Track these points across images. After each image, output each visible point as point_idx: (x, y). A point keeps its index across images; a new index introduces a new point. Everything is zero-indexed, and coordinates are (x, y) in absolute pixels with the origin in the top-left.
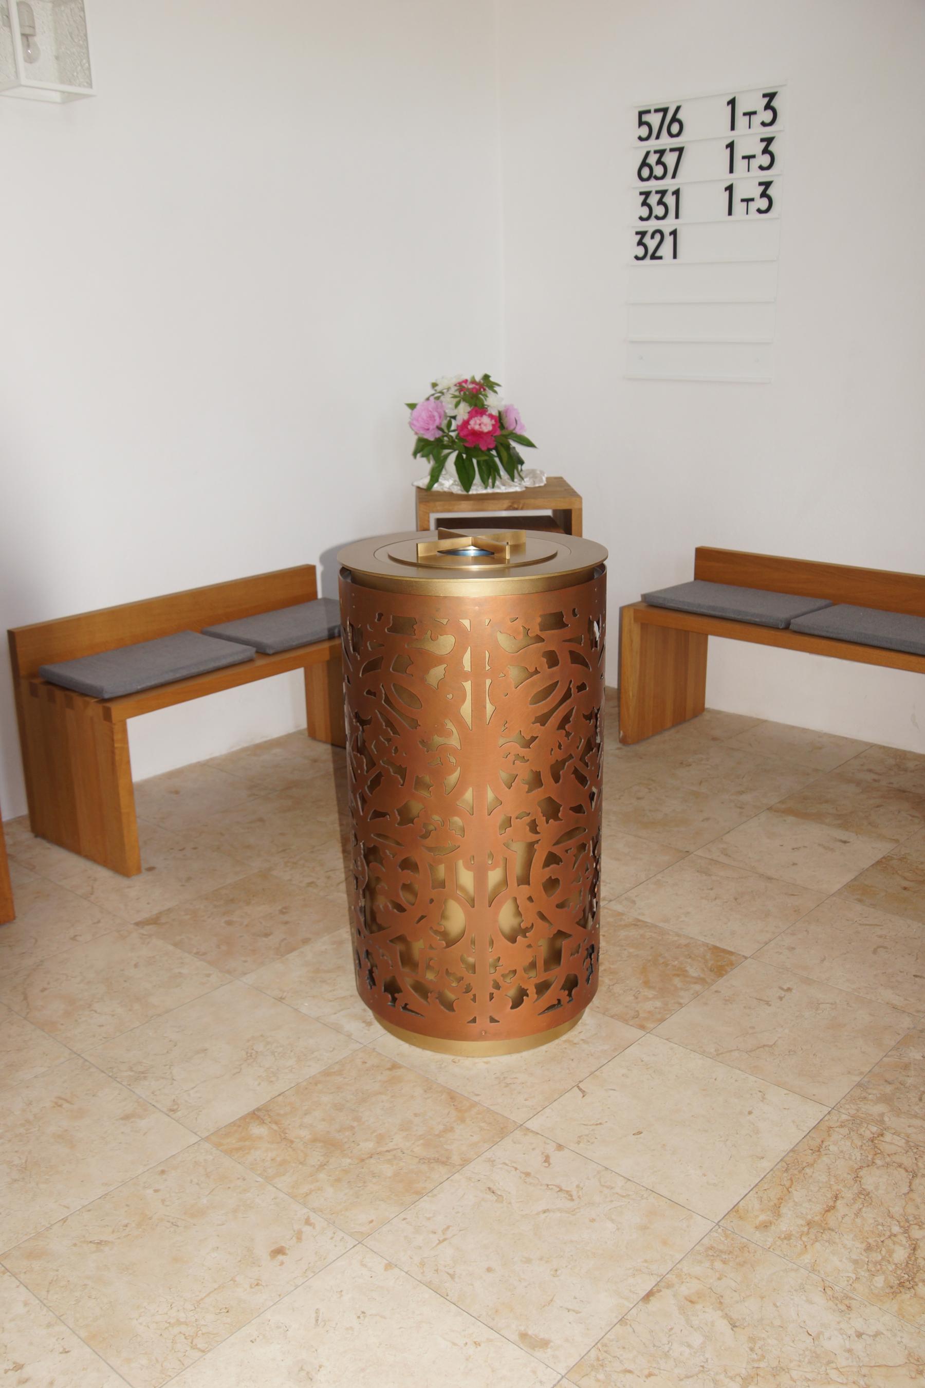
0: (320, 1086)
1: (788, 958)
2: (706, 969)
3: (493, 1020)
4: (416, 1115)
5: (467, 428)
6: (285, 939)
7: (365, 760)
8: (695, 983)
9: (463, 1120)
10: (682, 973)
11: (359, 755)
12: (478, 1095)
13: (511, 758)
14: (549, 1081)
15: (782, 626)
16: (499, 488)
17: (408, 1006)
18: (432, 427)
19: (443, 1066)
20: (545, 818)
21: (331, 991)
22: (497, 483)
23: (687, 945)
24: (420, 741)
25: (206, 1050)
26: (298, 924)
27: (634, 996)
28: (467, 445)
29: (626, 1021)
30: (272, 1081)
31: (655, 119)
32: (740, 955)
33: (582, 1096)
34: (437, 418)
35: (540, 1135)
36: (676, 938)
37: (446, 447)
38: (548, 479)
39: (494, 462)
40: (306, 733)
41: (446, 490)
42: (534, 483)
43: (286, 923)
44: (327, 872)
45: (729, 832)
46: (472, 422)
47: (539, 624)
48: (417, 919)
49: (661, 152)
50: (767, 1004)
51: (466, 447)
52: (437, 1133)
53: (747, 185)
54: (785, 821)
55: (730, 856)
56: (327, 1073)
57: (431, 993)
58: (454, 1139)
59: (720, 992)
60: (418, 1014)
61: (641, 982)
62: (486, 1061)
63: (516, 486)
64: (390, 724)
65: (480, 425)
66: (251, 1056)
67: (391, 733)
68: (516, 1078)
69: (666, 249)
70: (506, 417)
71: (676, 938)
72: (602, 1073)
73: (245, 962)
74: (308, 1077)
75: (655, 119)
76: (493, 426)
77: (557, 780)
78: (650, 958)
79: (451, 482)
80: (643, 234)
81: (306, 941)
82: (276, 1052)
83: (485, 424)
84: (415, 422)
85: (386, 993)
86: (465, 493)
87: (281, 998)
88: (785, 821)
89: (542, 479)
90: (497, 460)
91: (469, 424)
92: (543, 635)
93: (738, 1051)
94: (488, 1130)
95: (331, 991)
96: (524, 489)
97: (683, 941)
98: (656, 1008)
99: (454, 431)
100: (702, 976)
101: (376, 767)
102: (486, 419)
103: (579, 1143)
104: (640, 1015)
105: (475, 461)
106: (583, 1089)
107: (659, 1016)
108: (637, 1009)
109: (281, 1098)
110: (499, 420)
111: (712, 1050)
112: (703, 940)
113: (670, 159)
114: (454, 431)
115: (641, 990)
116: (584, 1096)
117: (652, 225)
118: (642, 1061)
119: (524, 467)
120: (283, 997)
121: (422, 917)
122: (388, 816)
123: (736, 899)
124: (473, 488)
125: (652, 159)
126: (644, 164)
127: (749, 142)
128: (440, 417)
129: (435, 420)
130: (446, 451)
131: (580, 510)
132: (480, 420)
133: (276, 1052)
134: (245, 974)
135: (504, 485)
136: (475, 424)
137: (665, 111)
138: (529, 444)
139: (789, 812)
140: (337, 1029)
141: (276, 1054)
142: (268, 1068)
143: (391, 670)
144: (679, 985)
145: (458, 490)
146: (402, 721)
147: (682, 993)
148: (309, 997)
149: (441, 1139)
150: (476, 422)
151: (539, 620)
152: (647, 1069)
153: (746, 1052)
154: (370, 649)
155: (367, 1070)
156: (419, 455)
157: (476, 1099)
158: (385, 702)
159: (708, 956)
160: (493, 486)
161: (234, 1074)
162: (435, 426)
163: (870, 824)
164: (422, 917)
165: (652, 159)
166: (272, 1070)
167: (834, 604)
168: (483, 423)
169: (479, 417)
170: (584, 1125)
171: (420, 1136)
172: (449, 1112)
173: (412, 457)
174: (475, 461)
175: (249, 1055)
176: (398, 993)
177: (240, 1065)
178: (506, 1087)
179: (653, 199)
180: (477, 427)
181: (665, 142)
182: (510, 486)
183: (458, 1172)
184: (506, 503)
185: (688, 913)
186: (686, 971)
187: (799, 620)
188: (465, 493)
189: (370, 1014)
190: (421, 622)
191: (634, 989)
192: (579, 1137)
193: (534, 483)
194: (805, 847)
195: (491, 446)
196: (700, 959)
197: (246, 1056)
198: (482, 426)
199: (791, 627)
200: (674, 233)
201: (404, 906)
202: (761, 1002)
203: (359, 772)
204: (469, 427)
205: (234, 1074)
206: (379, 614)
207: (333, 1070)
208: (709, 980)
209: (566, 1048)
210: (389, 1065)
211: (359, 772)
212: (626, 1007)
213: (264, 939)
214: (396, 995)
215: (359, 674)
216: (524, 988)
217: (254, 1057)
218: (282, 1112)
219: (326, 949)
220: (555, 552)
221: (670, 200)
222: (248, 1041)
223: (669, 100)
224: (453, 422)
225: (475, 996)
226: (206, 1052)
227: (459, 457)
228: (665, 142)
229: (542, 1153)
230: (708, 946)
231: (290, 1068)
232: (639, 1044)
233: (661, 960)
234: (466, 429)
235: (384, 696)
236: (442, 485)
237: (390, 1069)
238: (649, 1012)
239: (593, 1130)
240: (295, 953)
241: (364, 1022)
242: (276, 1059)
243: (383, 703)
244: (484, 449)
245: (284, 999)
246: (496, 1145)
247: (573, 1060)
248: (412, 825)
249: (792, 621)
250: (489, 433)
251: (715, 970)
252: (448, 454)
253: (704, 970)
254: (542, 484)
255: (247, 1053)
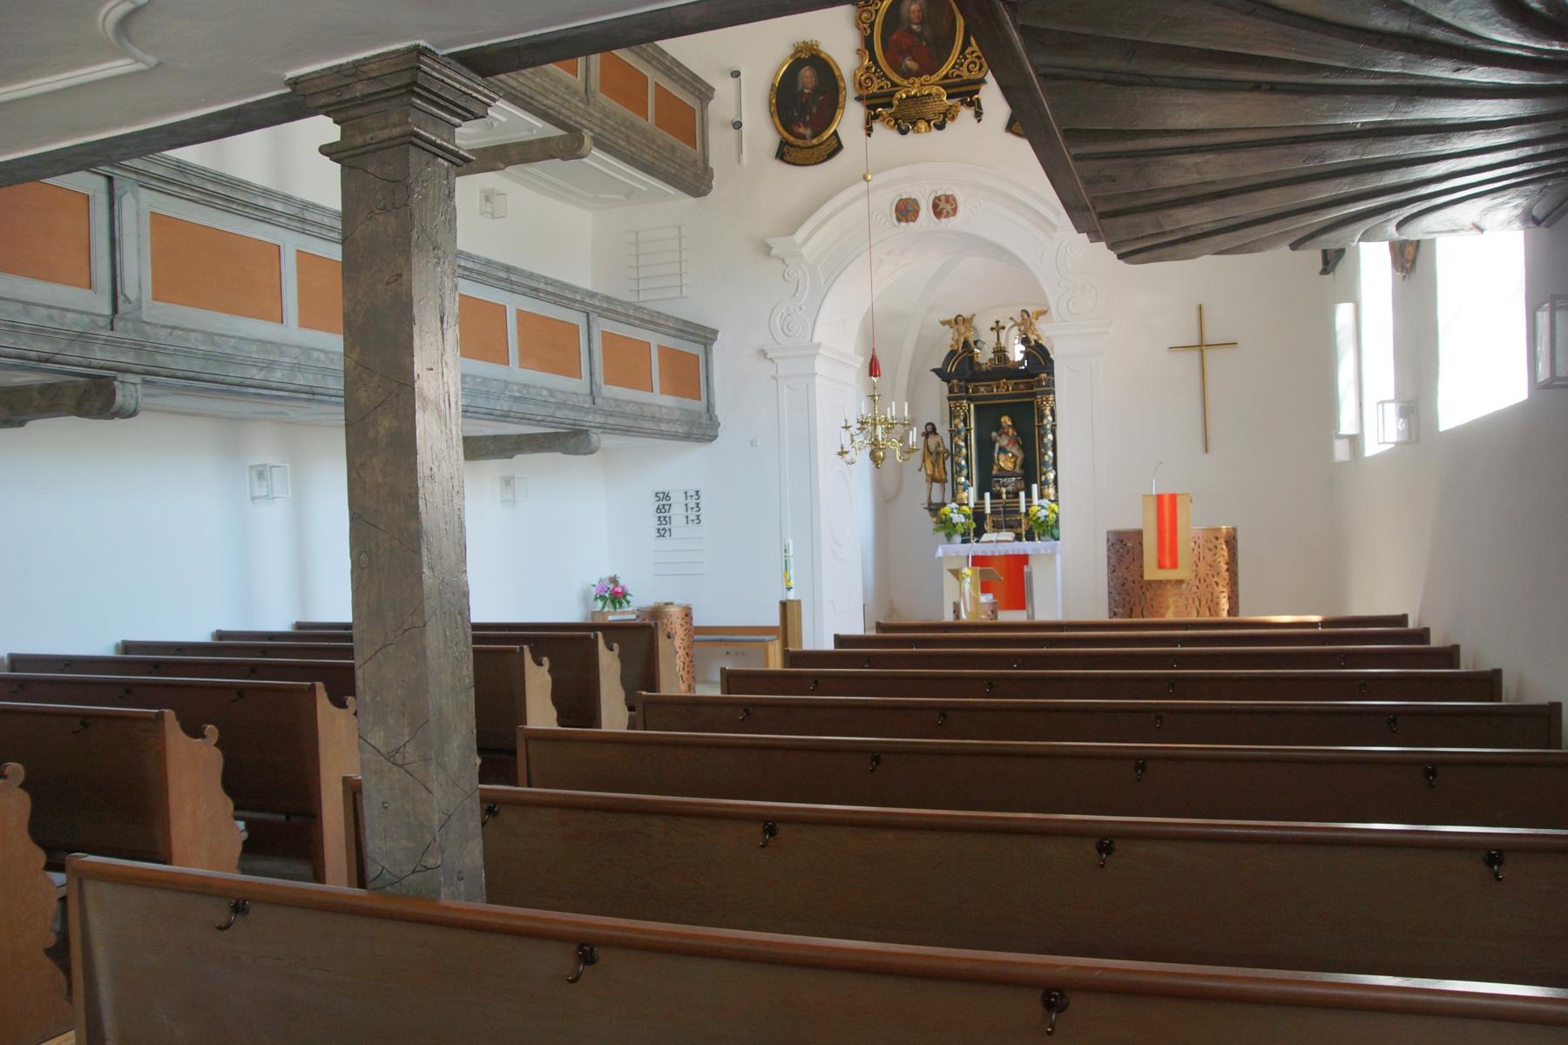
31: (661, 495)
49: (664, 505)
53: (692, 516)
69: (667, 534)
75: (661, 495)
80: (659, 529)
83: (620, 590)
92: (352, 709)
101: (150, 297)
110: (623, 588)
113: (667, 507)
117: (662, 527)
125: (661, 507)
126: (658, 508)
127: (692, 504)
136: (616, 589)
137: (664, 493)
165: (661, 507)
179: (662, 519)
181: (664, 502)
183: (592, 393)
200: (670, 529)
220: (934, 374)
221: (667, 519)
223: (666, 489)
228: (664, 502)
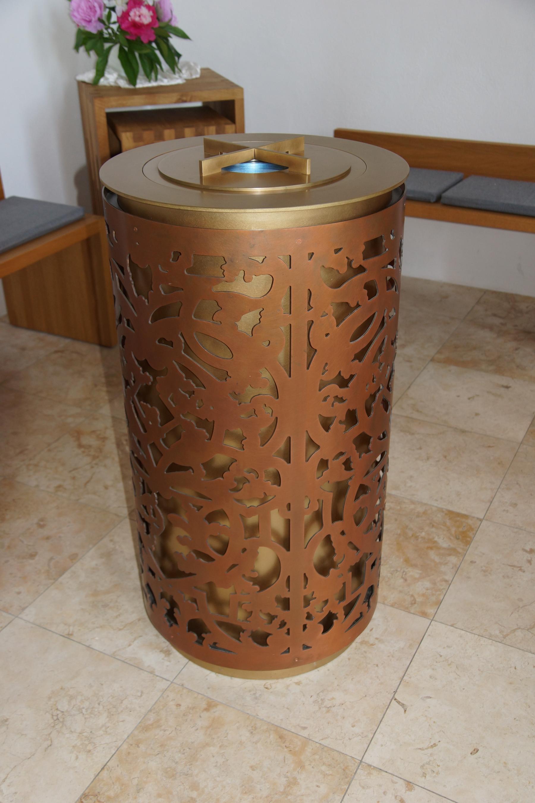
0: (142, 747)
1: (516, 516)
2: (452, 538)
3: (306, 647)
4: (253, 768)
5: (128, 20)
6: (52, 559)
7: (158, 412)
8: (450, 555)
9: (301, 765)
10: (433, 545)
11: (149, 406)
12: (305, 728)
13: (330, 400)
14: (366, 696)
15: (433, 200)
16: (162, 81)
17: (217, 645)
18: (94, 19)
19: (257, 695)
20: (358, 453)
21: (117, 617)
22: (159, 77)
23: (425, 513)
24: (230, 393)
25: (6, 720)
26: (60, 537)
27: (402, 577)
28: (128, 37)
29: (406, 609)
30: (90, 751)
32: (474, 517)
33: (403, 711)
34: (98, 9)
35: (384, 771)
36: (412, 506)
37: (107, 40)
38: (202, 70)
39: (155, 55)
40: (7, 320)
41: (112, 84)
42: (191, 75)
43: (48, 538)
44: (70, 471)
45: (409, 387)
46: (132, 14)
47: (363, 253)
48: (228, 568)
50: (521, 570)
51: (128, 40)
52: (282, 789)
54: (450, 371)
55: (421, 412)
56: (144, 727)
57: (243, 632)
58: (302, 795)
59: (475, 562)
60: (232, 652)
61: (402, 560)
62: (296, 681)
63: (177, 79)
64: (190, 374)
65: (140, 16)
66: (58, 719)
67: (194, 385)
68: (333, 698)
70: (161, 8)
71: (412, 506)
72: (410, 678)
73: (19, 593)
74: (126, 736)
76: (152, 17)
77: (369, 414)
78: (399, 531)
79: (115, 75)
81: (74, 557)
82: (83, 708)
84: (76, 14)
85: (190, 633)
86: (131, 87)
87: (69, 634)
88: (450, 371)
89: (196, 71)
90: (158, 53)
91: (129, 16)
93: (520, 630)
94: (331, 775)
95: (117, 617)
96: (184, 81)
97: (420, 509)
98: (427, 589)
99: (114, 23)
100: (452, 546)
102: (144, 11)
103: (424, 775)
104: (417, 600)
105: (137, 54)
106: (400, 701)
107: (433, 599)
108: (411, 593)
109: (105, 773)
111: (497, 632)
112: (436, 505)
114: (114, 23)
115: (406, 570)
116: (405, 711)
118: (441, 656)
119: (182, 60)
120: (70, 633)
121: (234, 566)
122: (191, 470)
123: (445, 457)
124: (138, 81)
128: (100, 8)
129: (95, 12)
130: (107, 45)
131: (242, 100)
132: (139, 11)
133: (83, 708)
134: (23, 609)
135: (166, 78)
136: (134, 15)
138: (183, 36)
139: (448, 361)
140: (138, 666)
141: (84, 710)
142: (80, 733)
143: (193, 317)
144: (437, 559)
145: (123, 84)
146: (196, 363)
147: (443, 568)
148: (97, 627)
149: (289, 797)
150: (135, 13)
151: (363, 248)
152: (449, 665)
153: (528, 630)
154: (163, 293)
155: (184, 715)
156: (82, 49)
157: (305, 733)
158: (184, 352)
159: (448, 523)
160: (156, 79)
161: (46, 749)
162: (96, 18)
163: (518, 367)
164: (234, 566)
166: (85, 734)
167: (466, 177)
168: (142, 14)
169: (138, 9)
170: (420, 749)
171: (266, 797)
172: (285, 757)
173: (73, 52)
174: (137, 54)
175: (55, 718)
176: (206, 633)
177: (50, 734)
178: (328, 712)
180: (137, 19)
182: (172, 79)
184: (175, 96)
185: (411, 477)
186: (435, 542)
187: (449, 194)
188: (131, 87)
189: (165, 643)
190: (232, 261)
191: (399, 569)
192: (422, 767)
193: (191, 75)
194: (478, 396)
195: (152, 39)
196: (442, 527)
197: (52, 721)
198: (142, 17)
199: (442, 200)
201: (212, 556)
202: (515, 568)
203: (151, 423)
204: (130, 19)
205: (46, 749)
206: (174, 253)
207: (150, 722)
208: (460, 551)
209: (365, 652)
210: (204, 705)
211: (151, 423)
212: (401, 592)
213: (31, 561)
214: (204, 635)
215: (148, 321)
216: (332, 613)
217: (61, 720)
218: (112, 793)
219: (97, 565)
222: (50, 698)
224: (113, 14)
225: (288, 630)
226: (7, 723)
227: (121, 50)
229: (396, 797)
230: (443, 512)
231: (104, 728)
232: (429, 635)
233: (410, 533)
234: (127, 21)
235: (183, 345)
236: (107, 79)
237: (207, 709)
238: (423, 595)
239: (431, 755)
240: (67, 575)
241: (161, 651)
242: (85, 718)
243: (183, 353)
244: (145, 41)
245: (72, 635)
246: (347, 795)
247: (377, 666)
248: (221, 479)
249: (444, 195)
250: (149, 25)
251: (460, 537)
252: (110, 48)
253: (450, 539)
254: (198, 76)
255: (53, 715)
